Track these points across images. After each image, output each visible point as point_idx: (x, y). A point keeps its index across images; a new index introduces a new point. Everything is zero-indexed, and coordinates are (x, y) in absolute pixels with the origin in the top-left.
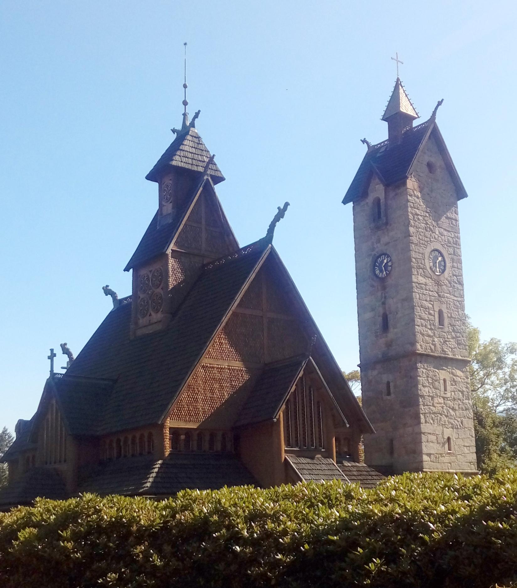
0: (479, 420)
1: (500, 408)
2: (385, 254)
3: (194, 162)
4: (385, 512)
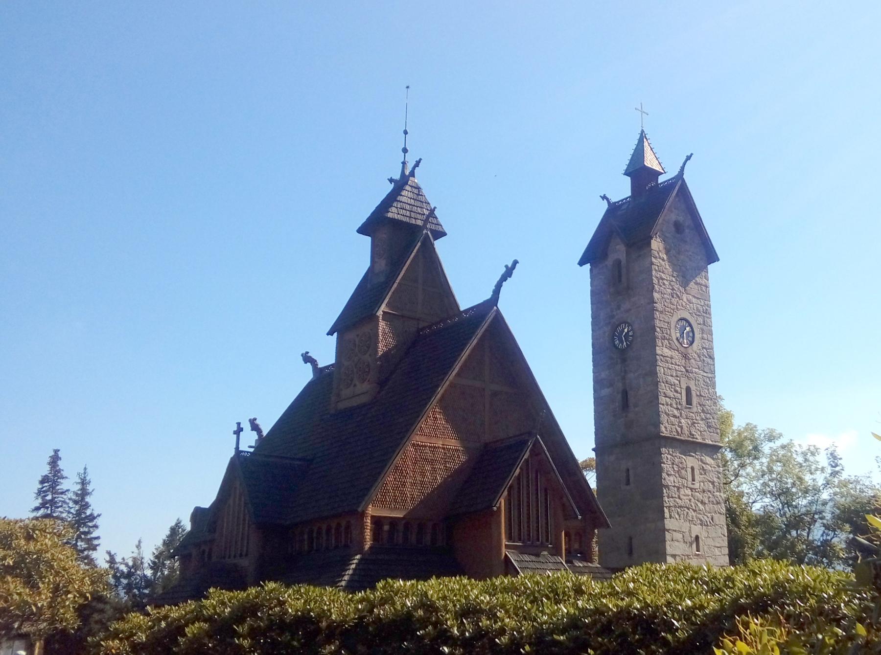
0: (732, 517)
2: (625, 323)
3: (413, 215)
4: (621, 607)
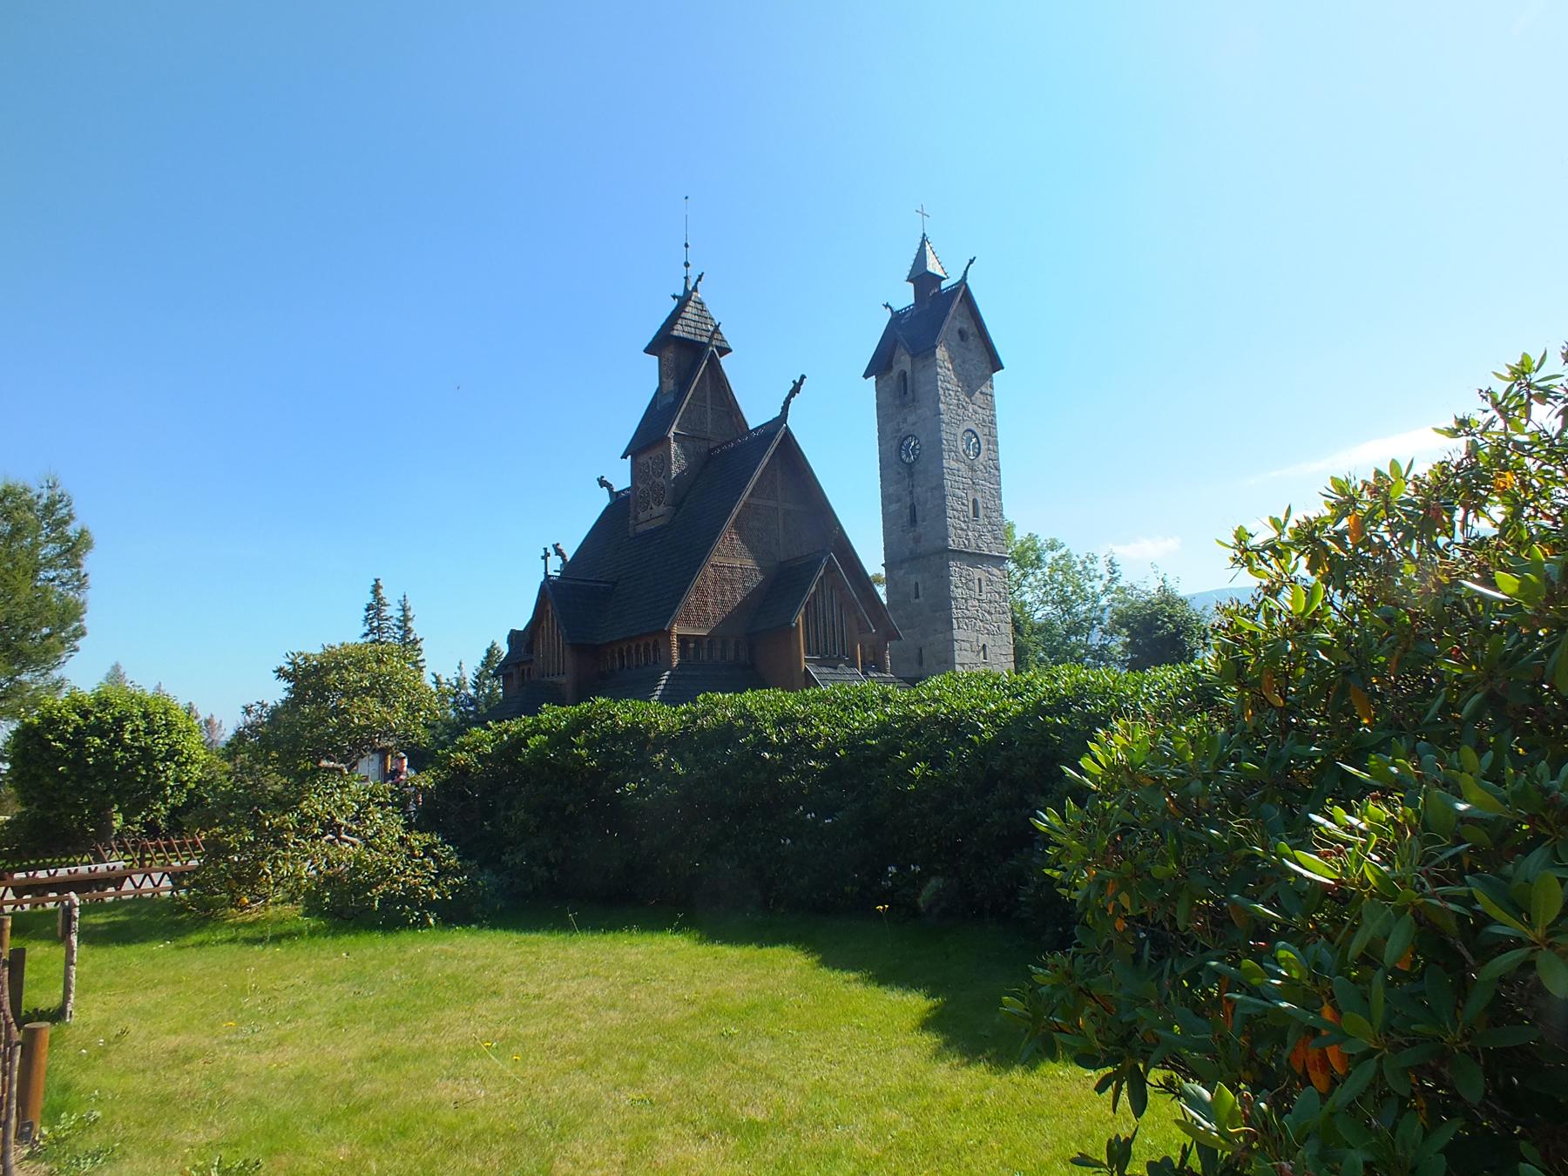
0: (1017, 628)
1: (1039, 614)
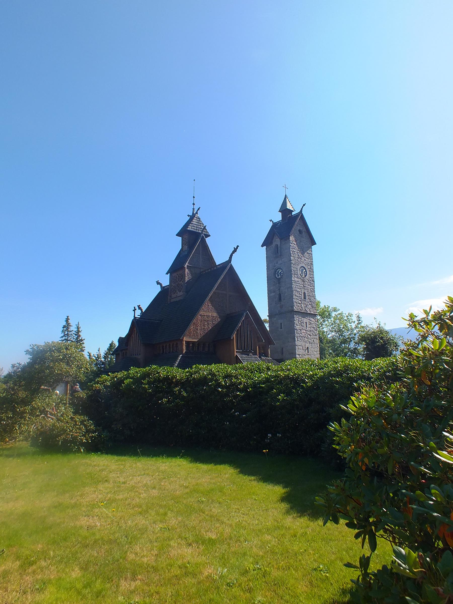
0: (321, 340)
1: (330, 336)
2: (280, 268)
